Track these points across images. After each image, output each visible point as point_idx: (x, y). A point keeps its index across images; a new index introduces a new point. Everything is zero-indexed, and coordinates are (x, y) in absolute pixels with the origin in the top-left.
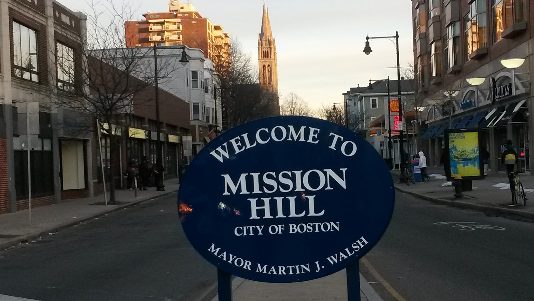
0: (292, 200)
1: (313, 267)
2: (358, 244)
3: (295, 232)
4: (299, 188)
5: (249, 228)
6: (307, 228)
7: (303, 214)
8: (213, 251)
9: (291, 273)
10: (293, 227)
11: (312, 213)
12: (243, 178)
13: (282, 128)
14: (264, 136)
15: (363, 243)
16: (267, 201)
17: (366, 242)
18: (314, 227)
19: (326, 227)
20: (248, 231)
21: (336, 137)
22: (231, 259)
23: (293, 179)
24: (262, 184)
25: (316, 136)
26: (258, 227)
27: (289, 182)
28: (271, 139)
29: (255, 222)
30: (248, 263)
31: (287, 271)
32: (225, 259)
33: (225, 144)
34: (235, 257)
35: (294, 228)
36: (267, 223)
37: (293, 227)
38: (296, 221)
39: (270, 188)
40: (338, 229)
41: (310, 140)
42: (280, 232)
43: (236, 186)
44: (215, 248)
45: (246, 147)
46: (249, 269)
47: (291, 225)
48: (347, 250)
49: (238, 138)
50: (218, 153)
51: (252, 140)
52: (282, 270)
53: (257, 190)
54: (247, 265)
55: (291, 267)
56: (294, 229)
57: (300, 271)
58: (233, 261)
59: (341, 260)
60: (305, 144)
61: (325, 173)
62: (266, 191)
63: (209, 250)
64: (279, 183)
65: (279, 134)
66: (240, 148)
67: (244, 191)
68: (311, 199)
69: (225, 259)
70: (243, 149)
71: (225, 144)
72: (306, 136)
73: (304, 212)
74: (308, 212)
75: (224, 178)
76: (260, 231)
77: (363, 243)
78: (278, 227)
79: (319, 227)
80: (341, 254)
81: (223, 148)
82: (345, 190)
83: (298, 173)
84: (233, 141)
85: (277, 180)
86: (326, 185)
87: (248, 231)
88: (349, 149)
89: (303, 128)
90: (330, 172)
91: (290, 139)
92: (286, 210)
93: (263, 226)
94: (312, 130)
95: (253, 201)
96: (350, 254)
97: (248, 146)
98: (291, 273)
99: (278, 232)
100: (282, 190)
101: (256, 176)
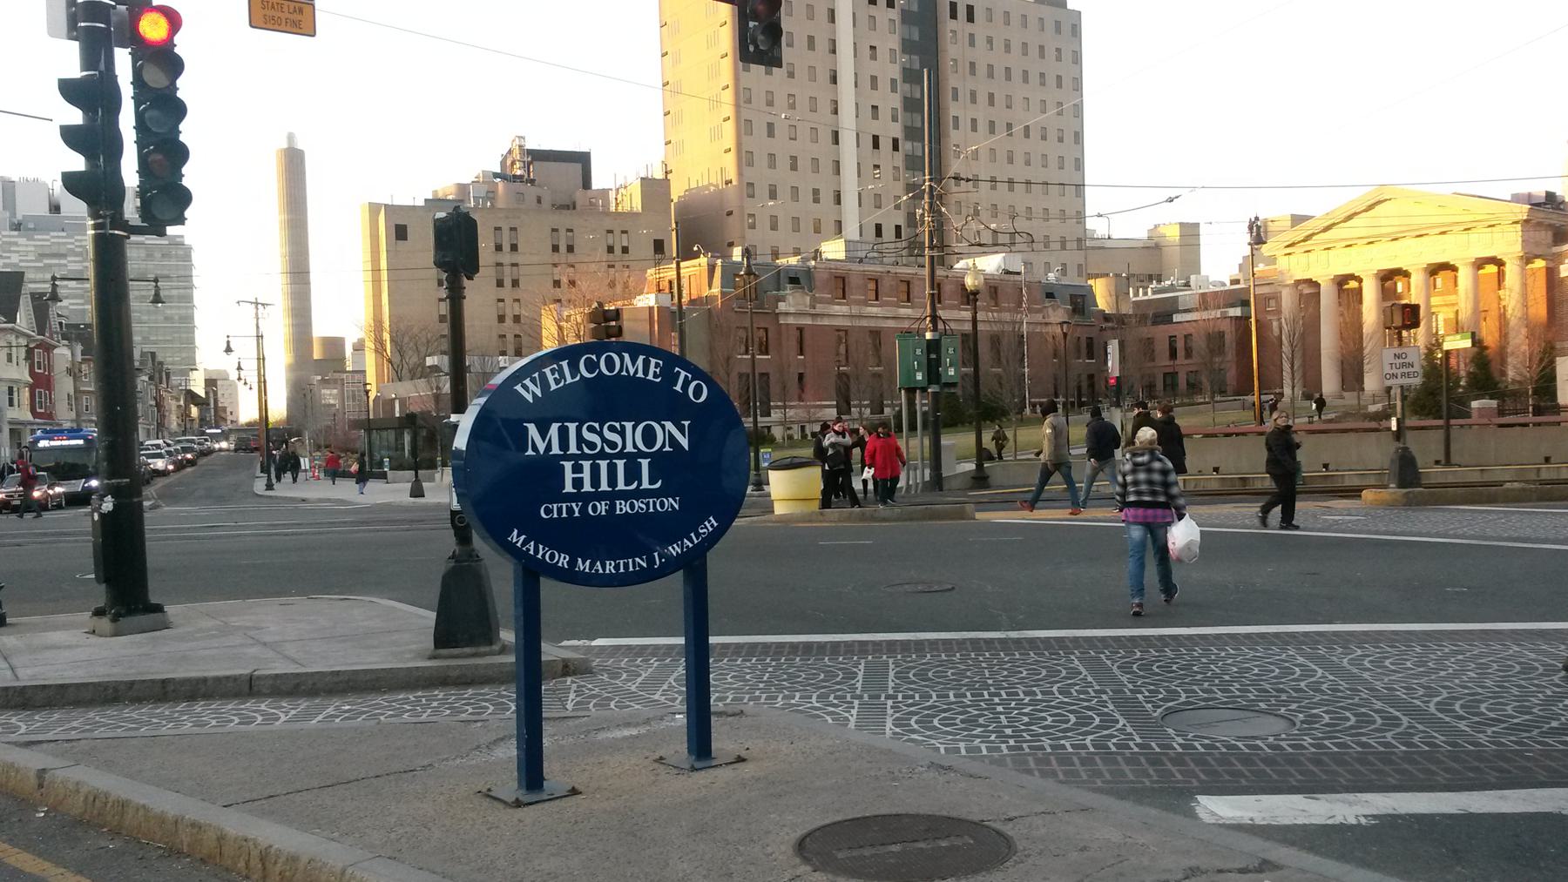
0: (620, 464)
1: (651, 561)
2: (706, 527)
3: (624, 512)
4: (630, 448)
5: (561, 506)
6: (639, 507)
8: (514, 541)
9: (622, 570)
10: (621, 504)
14: (591, 366)
15: (712, 526)
16: (586, 465)
17: (716, 524)
18: (647, 505)
20: (560, 510)
21: (683, 373)
22: (541, 553)
23: (622, 433)
24: (581, 440)
25: (658, 370)
26: (574, 505)
29: (570, 498)
30: (565, 558)
31: (617, 567)
32: (532, 552)
33: (536, 375)
34: (547, 549)
35: (622, 506)
36: (585, 498)
37: (621, 504)
38: (625, 496)
39: (592, 445)
40: (677, 507)
41: (650, 377)
42: (603, 513)
43: (544, 442)
44: (518, 536)
45: (565, 381)
46: (566, 567)
47: (618, 502)
48: (692, 535)
49: (555, 366)
50: (526, 388)
52: (610, 567)
53: (573, 449)
54: (563, 560)
55: (622, 562)
56: (622, 507)
57: (634, 567)
58: (544, 555)
59: (685, 550)
60: (644, 381)
61: (663, 427)
62: (586, 451)
63: (509, 539)
64: (604, 440)
65: (610, 364)
66: (557, 382)
67: (556, 450)
68: (645, 463)
69: (532, 552)
70: (562, 384)
71: (536, 375)
72: (646, 372)
73: (636, 483)
74: (640, 484)
75: (526, 428)
76: (576, 510)
77: (712, 526)
78: (601, 504)
79: (654, 503)
80: (685, 541)
81: (533, 381)
84: (547, 371)
85: (600, 434)
86: (663, 445)
87: (560, 510)
89: (641, 358)
91: (624, 373)
92: (612, 480)
93: (580, 504)
94: (653, 361)
95: (568, 465)
96: (696, 542)
97: (569, 380)
98: (622, 570)
99: (601, 512)
100: (607, 450)
101: (572, 427)
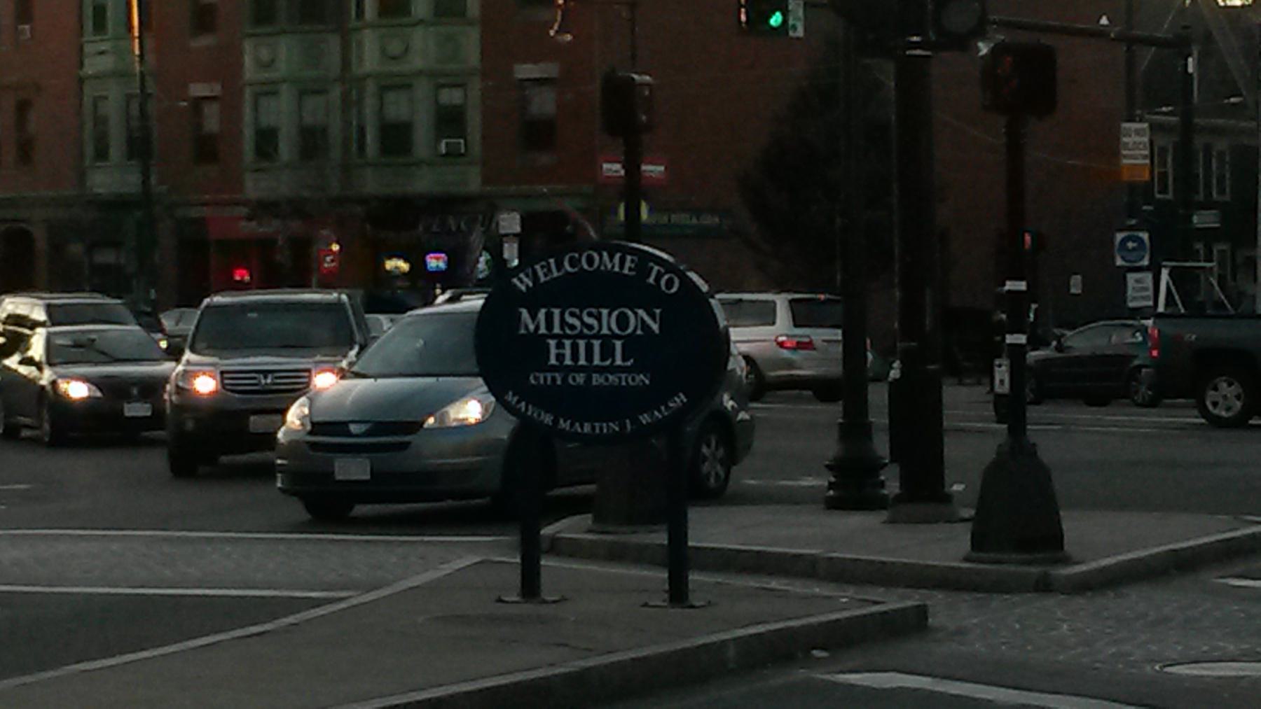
0: (597, 344)
4: (605, 331)
7: (608, 363)
11: (619, 362)
12: (542, 315)
16: (567, 343)
18: (620, 379)
19: (633, 379)
20: (545, 379)
23: (599, 318)
24: (563, 323)
25: (633, 266)
27: (571, 320)
31: (593, 428)
38: (601, 370)
39: (572, 327)
41: (626, 271)
51: (559, 266)
53: (557, 330)
56: (597, 379)
62: (568, 332)
64: (583, 323)
65: (590, 261)
66: (546, 275)
67: (543, 330)
74: (614, 361)
79: (626, 378)
82: (657, 335)
83: (605, 312)
84: (537, 267)
88: (670, 283)
90: (641, 312)
92: (589, 357)
94: (629, 258)
95: (552, 343)
97: (556, 274)
101: (557, 312)
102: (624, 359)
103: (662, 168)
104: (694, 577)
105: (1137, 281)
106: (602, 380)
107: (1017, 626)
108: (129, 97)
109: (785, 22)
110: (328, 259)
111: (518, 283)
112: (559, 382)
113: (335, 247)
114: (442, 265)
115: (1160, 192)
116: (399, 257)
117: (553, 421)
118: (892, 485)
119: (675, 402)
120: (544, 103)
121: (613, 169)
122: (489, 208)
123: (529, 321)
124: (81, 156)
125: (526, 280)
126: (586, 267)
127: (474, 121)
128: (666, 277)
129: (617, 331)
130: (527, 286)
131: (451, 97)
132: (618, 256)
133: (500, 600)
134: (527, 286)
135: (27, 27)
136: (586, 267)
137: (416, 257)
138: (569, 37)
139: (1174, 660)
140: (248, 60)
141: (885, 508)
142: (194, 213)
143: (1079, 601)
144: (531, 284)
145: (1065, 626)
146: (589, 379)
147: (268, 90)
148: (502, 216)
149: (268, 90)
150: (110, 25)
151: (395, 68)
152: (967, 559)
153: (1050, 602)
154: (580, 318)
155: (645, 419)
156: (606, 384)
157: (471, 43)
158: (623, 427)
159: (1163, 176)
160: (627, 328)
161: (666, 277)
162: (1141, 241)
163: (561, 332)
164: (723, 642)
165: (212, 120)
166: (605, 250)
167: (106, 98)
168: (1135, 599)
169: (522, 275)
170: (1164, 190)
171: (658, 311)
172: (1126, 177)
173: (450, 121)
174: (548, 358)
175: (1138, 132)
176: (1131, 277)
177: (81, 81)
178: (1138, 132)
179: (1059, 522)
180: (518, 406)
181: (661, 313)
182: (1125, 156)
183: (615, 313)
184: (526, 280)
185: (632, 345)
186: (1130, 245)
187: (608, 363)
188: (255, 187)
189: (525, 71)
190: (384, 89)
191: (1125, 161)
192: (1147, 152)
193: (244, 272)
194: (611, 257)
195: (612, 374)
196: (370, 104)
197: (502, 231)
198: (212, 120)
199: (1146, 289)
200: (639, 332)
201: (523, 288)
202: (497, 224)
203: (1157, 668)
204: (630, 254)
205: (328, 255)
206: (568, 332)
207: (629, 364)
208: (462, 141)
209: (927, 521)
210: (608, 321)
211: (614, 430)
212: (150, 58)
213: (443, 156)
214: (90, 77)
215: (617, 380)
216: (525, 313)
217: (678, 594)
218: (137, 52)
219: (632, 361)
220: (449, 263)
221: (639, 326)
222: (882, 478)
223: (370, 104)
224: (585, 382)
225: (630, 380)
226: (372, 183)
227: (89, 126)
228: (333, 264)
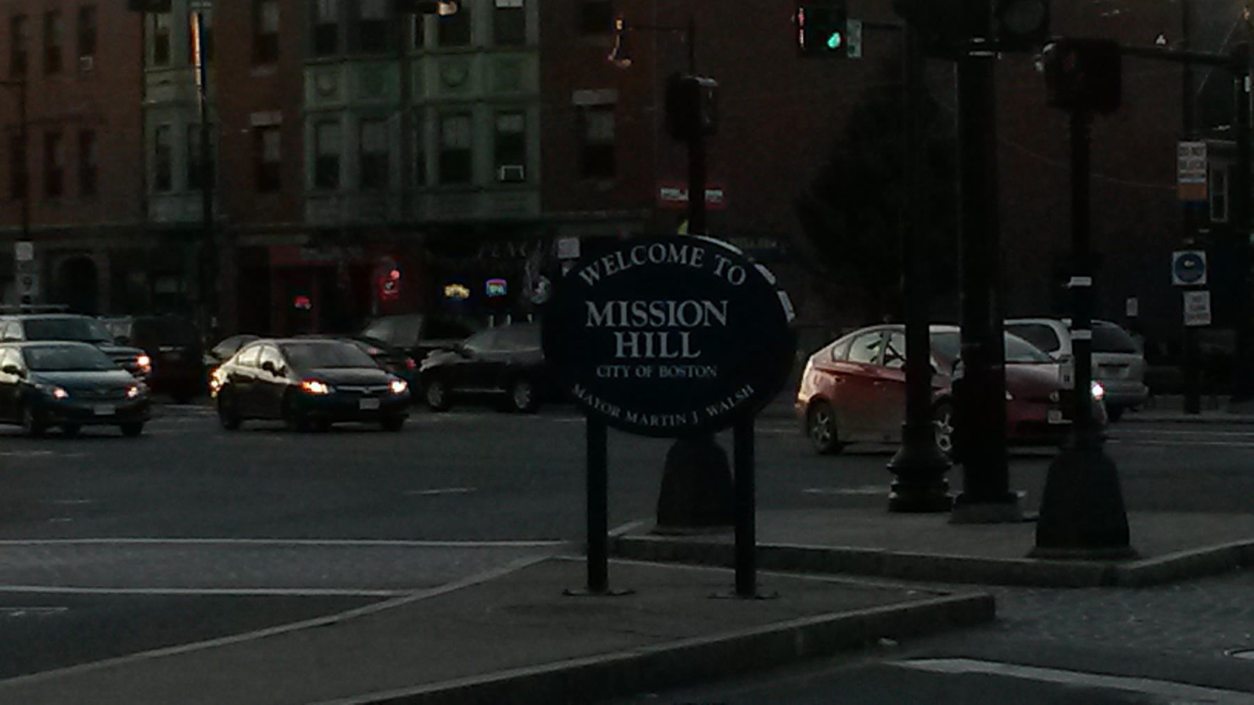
0: (664, 336)
4: (672, 323)
7: (676, 354)
11: (686, 354)
13: (661, 247)
16: (634, 336)
18: (687, 371)
19: (701, 371)
20: (612, 371)
24: (630, 315)
25: (700, 258)
26: (624, 367)
27: (661, 315)
28: (649, 259)
29: (619, 361)
31: (660, 421)
38: (665, 361)
39: (639, 319)
42: (649, 376)
51: (627, 259)
53: (624, 323)
54: (615, 412)
56: (664, 372)
58: (599, 406)
62: (635, 324)
65: (657, 253)
67: (610, 323)
68: (685, 336)
72: (689, 258)
74: (681, 351)
77: (749, 392)
83: (672, 304)
84: (605, 260)
88: (737, 275)
90: (708, 304)
94: (696, 250)
95: (619, 336)
97: (623, 267)
100: (653, 324)
101: (624, 305)
102: (691, 351)
103: (720, 193)
104: (762, 575)
105: (1195, 299)
106: (669, 372)
107: (1085, 618)
108: (190, 128)
109: (843, 41)
110: (389, 285)
111: (585, 277)
112: (626, 375)
113: (396, 274)
114: (501, 290)
115: (1214, 217)
116: (458, 283)
117: (620, 414)
118: (954, 483)
119: (742, 394)
120: (603, 129)
121: (673, 194)
122: (547, 233)
123: (596, 314)
124: (144, 183)
125: (592, 273)
126: (652, 259)
127: (533, 148)
128: (732, 269)
129: (684, 323)
130: (594, 280)
131: (510, 124)
132: (685, 247)
133: (567, 593)
134: (594, 280)
135: (90, 59)
136: (652, 259)
137: (476, 284)
138: (627, 62)
139: (1243, 647)
140: (309, 84)
141: (949, 510)
142: (253, 240)
143: (1145, 594)
144: (597, 277)
145: (1133, 618)
146: (655, 372)
147: (327, 118)
148: (562, 241)
149: (327, 118)
150: (172, 53)
151: (454, 95)
152: (1031, 556)
153: (1118, 595)
154: (647, 310)
155: (712, 411)
156: (674, 367)
157: (530, 70)
158: (690, 418)
159: (1219, 201)
160: (693, 321)
161: (732, 269)
162: (1198, 259)
163: (628, 325)
164: (792, 629)
165: (273, 150)
166: (672, 242)
167: (166, 127)
168: (1202, 593)
169: (589, 269)
170: (1219, 213)
171: (725, 303)
172: (1183, 195)
173: (509, 147)
174: (615, 352)
175: (1195, 151)
176: (1189, 297)
177: (143, 111)
178: (1195, 151)
179: (1126, 523)
180: (585, 399)
181: (728, 305)
182: (1183, 176)
183: (683, 305)
184: (592, 273)
185: (698, 337)
186: (1187, 263)
187: (676, 354)
188: (316, 214)
189: (584, 97)
190: (442, 118)
191: (1183, 180)
192: (1204, 171)
193: (307, 300)
194: (678, 250)
195: (678, 365)
196: (430, 126)
197: (560, 256)
198: (273, 150)
199: (1203, 308)
200: (706, 324)
201: (590, 281)
202: (557, 246)
203: (1226, 653)
204: (697, 246)
205: (389, 282)
206: (635, 324)
207: (697, 355)
208: (521, 167)
209: (993, 521)
210: (675, 314)
211: (681, 422)
212: (212, 88)
213: (503, 181)
214: (152, 105)
215: (684, 372)
216: (592, 307)
217: (745, 587)
218: (199, 82)
219: (699, 353)
220: (508, 289)
221: (706, 318)
222: (946, 480)
223: (430, 126)
224: (651, 374)
225: (697, 373)
226: (430, 210)
227: (151, 153)
228: (393, 291)
